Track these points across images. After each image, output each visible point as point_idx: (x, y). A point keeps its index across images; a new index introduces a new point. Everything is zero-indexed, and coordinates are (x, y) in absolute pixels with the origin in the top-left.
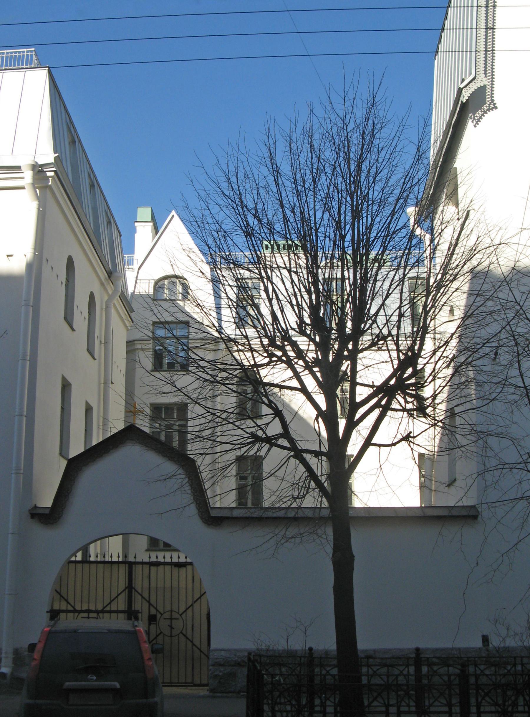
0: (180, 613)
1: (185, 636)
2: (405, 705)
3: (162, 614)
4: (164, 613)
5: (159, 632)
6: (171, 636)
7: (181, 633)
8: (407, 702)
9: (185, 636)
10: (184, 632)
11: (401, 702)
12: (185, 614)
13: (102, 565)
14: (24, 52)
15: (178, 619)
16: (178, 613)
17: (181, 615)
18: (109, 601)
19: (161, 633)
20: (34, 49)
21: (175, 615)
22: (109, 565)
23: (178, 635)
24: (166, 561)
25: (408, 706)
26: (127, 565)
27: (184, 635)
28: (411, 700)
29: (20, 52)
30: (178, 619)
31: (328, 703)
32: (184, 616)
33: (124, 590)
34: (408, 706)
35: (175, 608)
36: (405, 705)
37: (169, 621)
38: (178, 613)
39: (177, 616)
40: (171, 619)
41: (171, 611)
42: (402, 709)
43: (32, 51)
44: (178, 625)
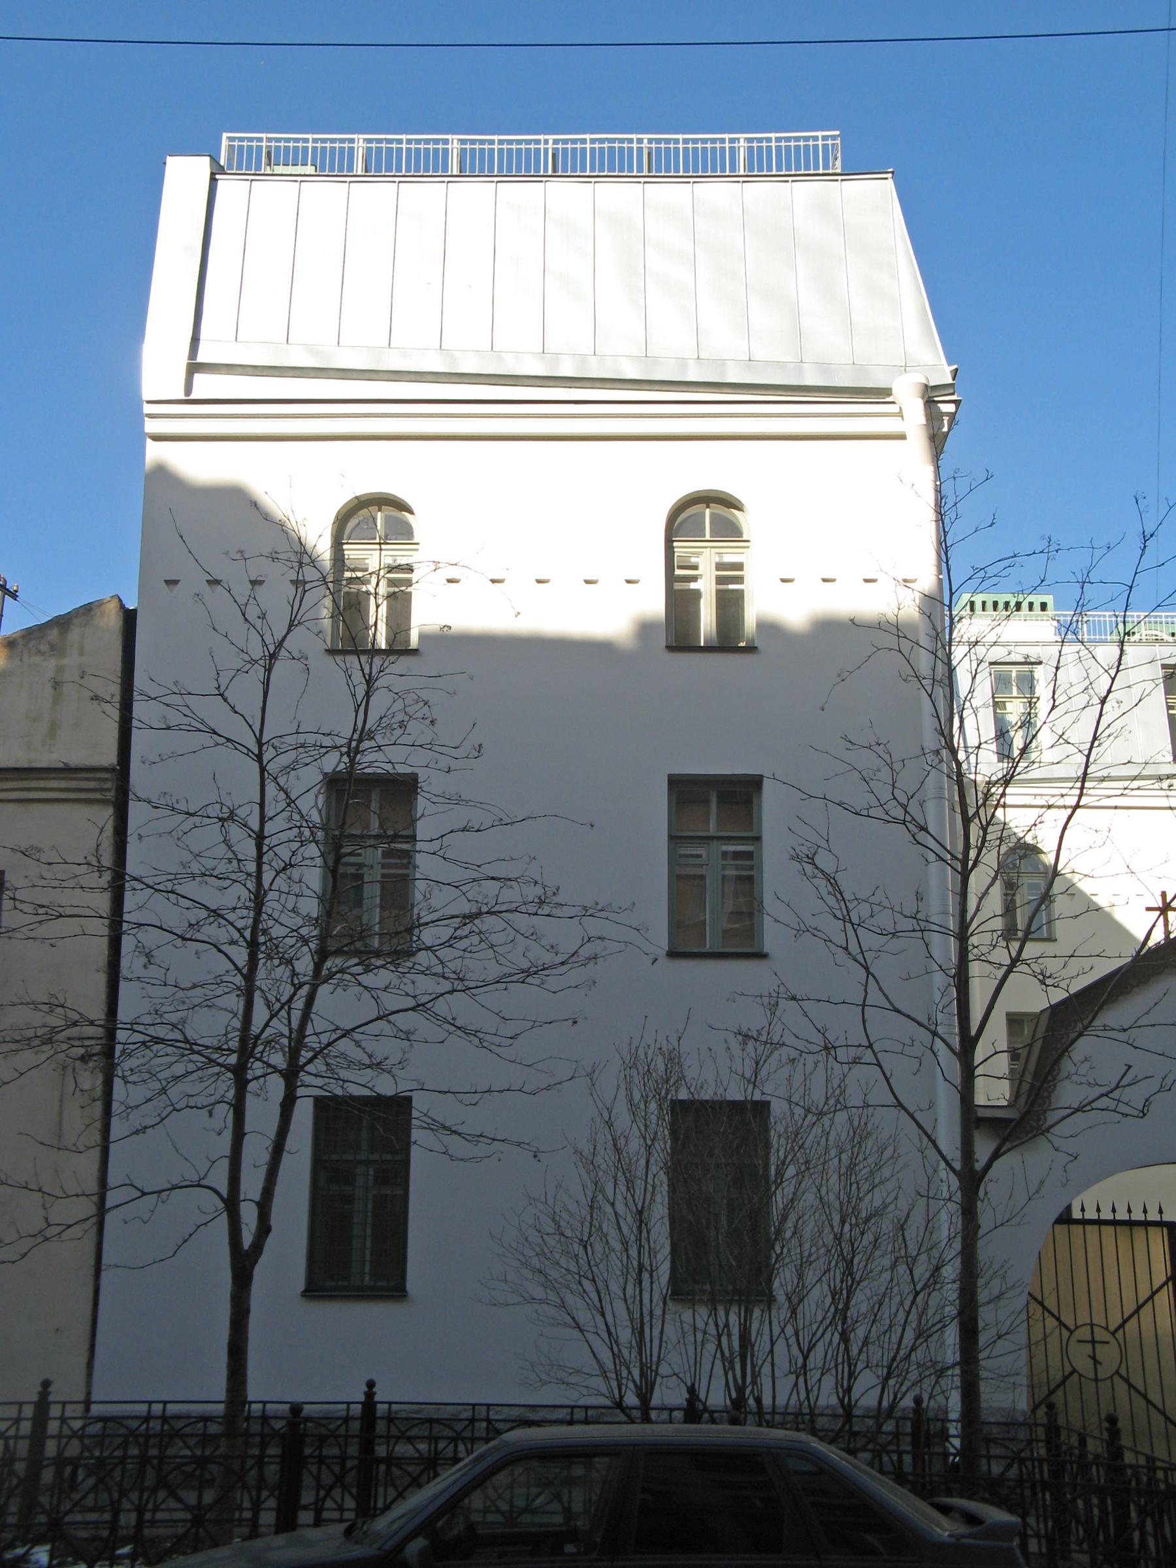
0: (1112, 1328)
1: (1126, 1380)
2: (335, 1506)
3: (1071, 1332)
4: (1077, 1328)
5: (1068, 1369)
6: (1096, 1380)
7: (1117, 1372)
8: (339, 1500)
9: (1126, 1380)
10: (1123, 1372)
11: (324, 1499)
12: (1121, 1332)
13: (1111, 1229)
14: (260, 140)
15: (1108, 1343)
16: (1107, 1329)
17: (1113, 1333)
18: (1142, 1312)
19: (1074, 1371)
20: (837, 133)
21: (1100, 1334)
22: (1126, 1229)
23: (1111, 1377)
24: (1133, 1218)
25: (341, 1509)
26: (1165, 1230)
27: (1121, 1377)
28: (347, 1495)
29: (574, 141)
30: (1108, 1343)
31: (126, 1505)
32: (1120, 1334)
33: (1166, 1283)
34: (341, 1509)
35: (1099, 1319)
36: (335, 1506)
37: (1090, 1346)
38: (1107, 1329)
39: (1106, 1336)
40: (1093, 1342)
41: (1092, 1325)
42: (325, 1515)
43: (834, 138)
44: (1109, 1356)
